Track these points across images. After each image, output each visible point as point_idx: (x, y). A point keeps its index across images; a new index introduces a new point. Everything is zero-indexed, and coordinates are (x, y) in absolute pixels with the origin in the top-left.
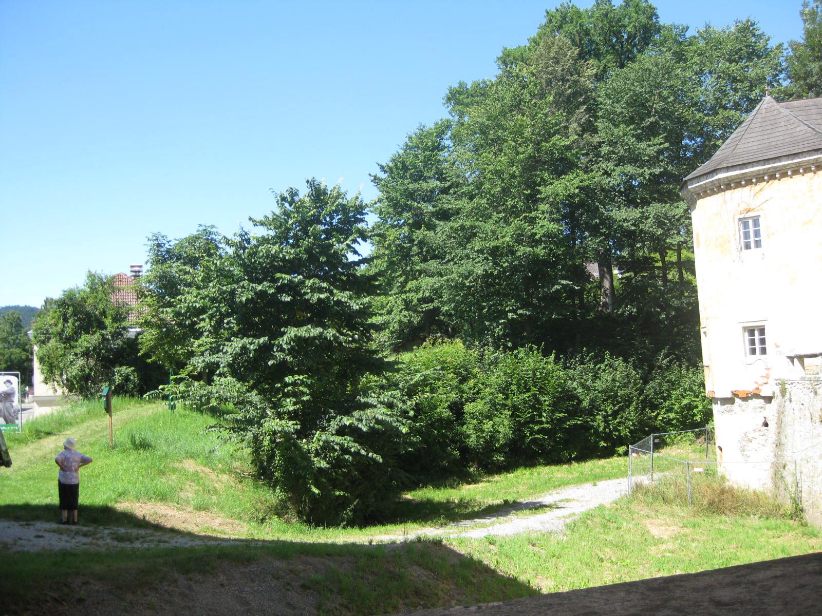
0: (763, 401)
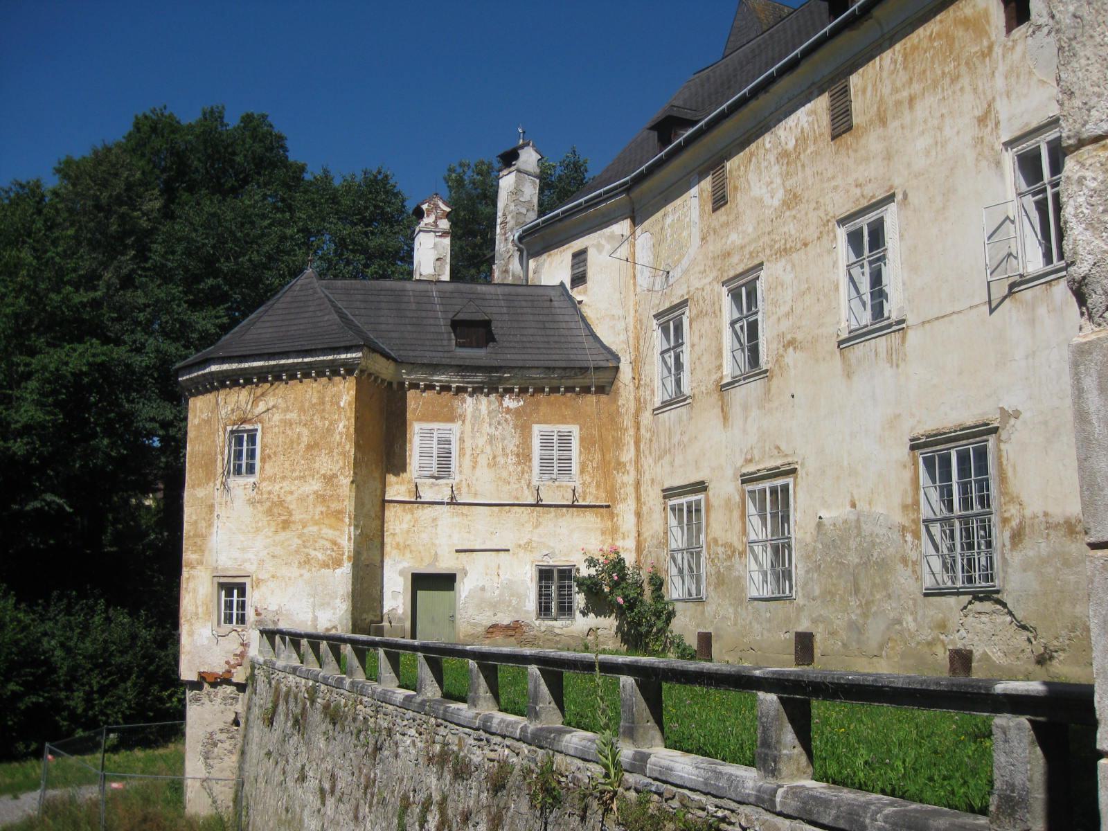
0: (235, 688)
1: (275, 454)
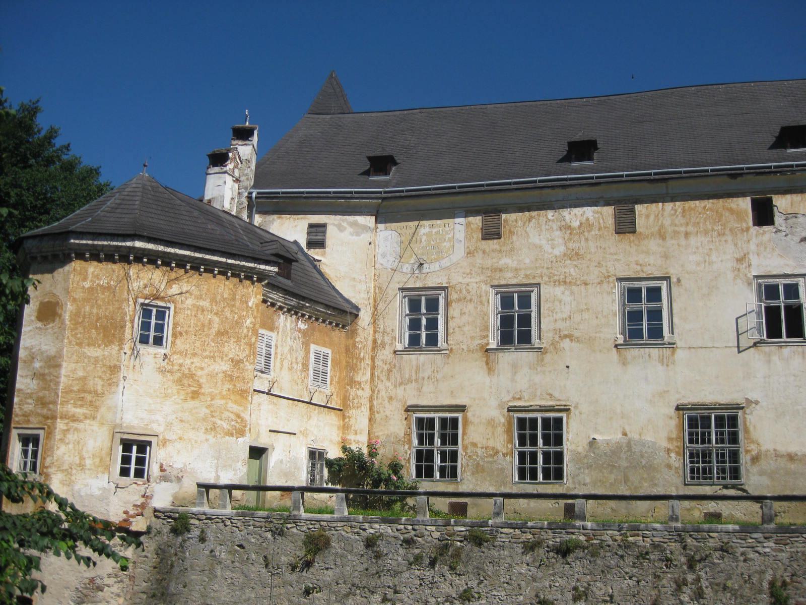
1: (187, 332)
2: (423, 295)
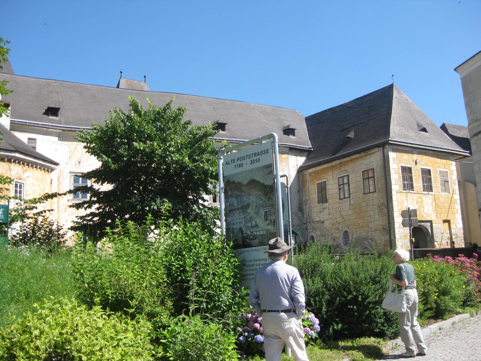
2: (221, 205)
